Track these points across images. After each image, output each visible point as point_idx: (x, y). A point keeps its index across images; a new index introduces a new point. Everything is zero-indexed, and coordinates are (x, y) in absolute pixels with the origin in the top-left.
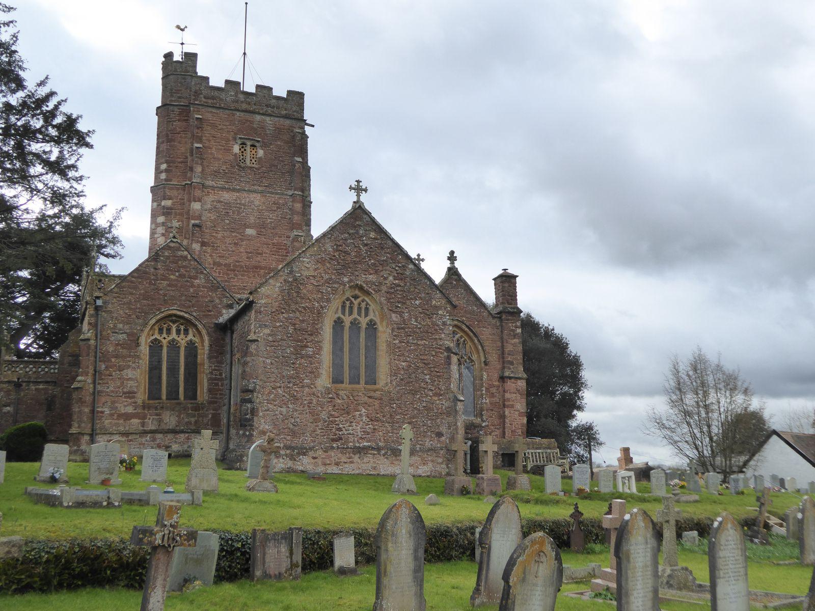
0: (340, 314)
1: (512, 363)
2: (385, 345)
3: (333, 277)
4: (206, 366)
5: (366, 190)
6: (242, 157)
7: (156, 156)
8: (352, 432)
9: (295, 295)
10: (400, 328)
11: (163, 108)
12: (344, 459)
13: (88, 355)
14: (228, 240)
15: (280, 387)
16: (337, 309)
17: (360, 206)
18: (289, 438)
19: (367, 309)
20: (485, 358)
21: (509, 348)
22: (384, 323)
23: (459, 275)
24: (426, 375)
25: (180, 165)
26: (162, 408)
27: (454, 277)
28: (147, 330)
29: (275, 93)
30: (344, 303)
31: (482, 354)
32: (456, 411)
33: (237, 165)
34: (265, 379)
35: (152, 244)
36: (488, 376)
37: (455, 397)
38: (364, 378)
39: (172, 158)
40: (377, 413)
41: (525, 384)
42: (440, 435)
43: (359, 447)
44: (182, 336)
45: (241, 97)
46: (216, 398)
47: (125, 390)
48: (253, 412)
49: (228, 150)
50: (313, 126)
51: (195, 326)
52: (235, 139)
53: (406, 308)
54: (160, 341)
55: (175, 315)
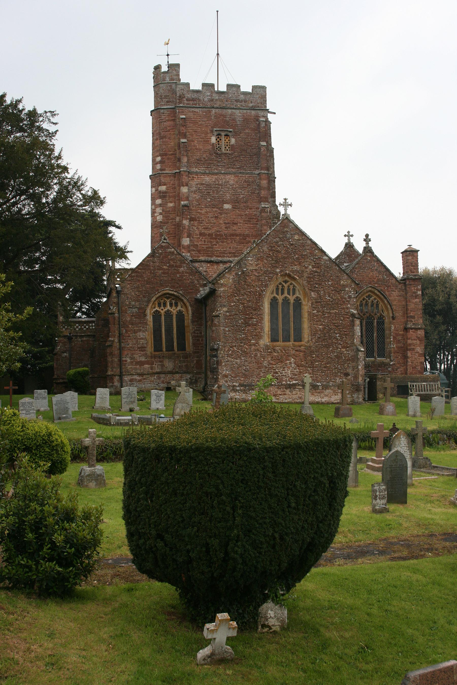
0: (275, 295)
1: (413, 317)
2: (307, 314)
3: (269, 269)
4: (191, 328)
5: (291, 205)
6: (218, 146)
7: (152, 150)
8: (284, 374)
9: (243, 283)
10: (317, 303)
11: (156, 111)
12: (279, 392)
13: (114, 324)
14: (210, 215)
15: (235, 346)
16: (273, 291)
17: (287, 218)
18: (242, 379)
19: (294, 290)
20: (393, 314)
21: (411, 306)
22: (306, 299)
23: (372, 253)
24: (337, 334)
25: (171, 157)
26: (163, 357)
27: (368, 254)
28: (151, 305)
29: (243, 89)
30: (278, 286)
31: (390, 312)
32: (358, 359)
33: (215, 153)
34: (225, 341)
35: (153, 221)
36: (395, 328)
37: (357, 349)
38: (293, 337)
39: (165, 151)
40: (302, 361)
41: (423, 333)
42: (347, 375)
43: (290, 385)
44: (174, 307)
45: (216, 97)
46: (198, 349)
47: (139, 346)
48: (218, 363)
49: (207, 141)
50: (275, 113)
51: (182, 301)
52: (212, 131)
53: (322, 288)
54: (159, 312)
55: (168, 294)
